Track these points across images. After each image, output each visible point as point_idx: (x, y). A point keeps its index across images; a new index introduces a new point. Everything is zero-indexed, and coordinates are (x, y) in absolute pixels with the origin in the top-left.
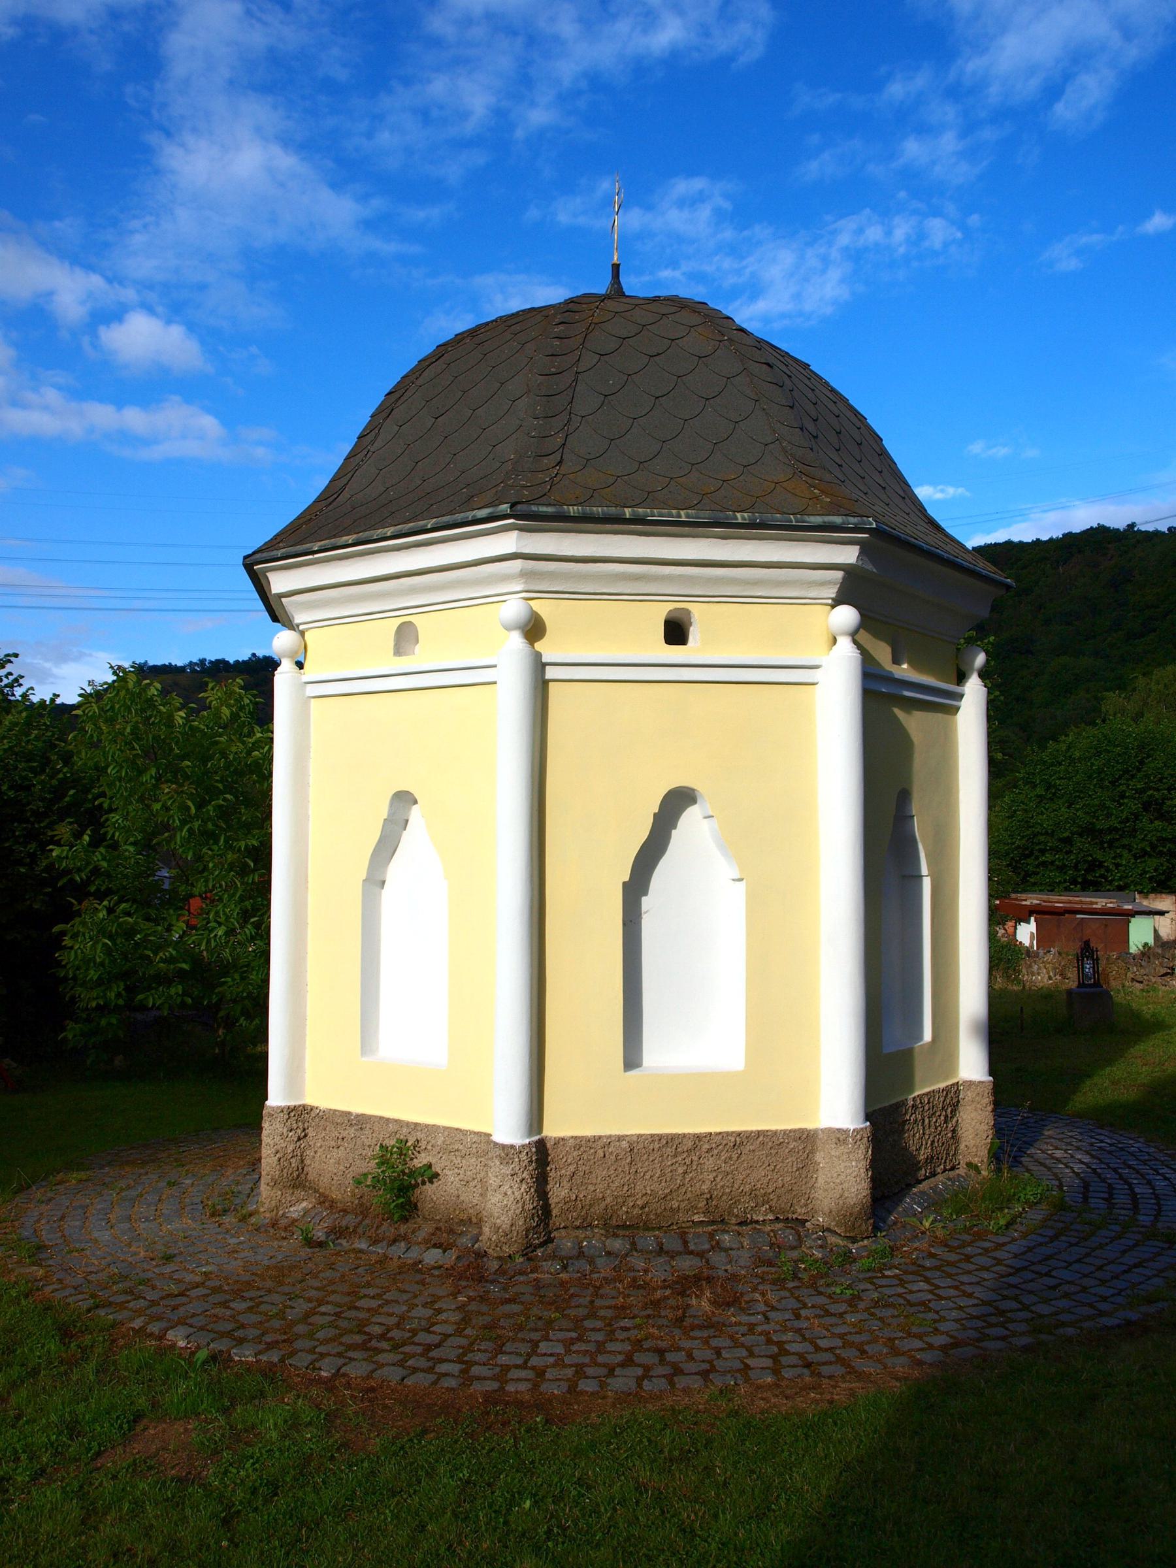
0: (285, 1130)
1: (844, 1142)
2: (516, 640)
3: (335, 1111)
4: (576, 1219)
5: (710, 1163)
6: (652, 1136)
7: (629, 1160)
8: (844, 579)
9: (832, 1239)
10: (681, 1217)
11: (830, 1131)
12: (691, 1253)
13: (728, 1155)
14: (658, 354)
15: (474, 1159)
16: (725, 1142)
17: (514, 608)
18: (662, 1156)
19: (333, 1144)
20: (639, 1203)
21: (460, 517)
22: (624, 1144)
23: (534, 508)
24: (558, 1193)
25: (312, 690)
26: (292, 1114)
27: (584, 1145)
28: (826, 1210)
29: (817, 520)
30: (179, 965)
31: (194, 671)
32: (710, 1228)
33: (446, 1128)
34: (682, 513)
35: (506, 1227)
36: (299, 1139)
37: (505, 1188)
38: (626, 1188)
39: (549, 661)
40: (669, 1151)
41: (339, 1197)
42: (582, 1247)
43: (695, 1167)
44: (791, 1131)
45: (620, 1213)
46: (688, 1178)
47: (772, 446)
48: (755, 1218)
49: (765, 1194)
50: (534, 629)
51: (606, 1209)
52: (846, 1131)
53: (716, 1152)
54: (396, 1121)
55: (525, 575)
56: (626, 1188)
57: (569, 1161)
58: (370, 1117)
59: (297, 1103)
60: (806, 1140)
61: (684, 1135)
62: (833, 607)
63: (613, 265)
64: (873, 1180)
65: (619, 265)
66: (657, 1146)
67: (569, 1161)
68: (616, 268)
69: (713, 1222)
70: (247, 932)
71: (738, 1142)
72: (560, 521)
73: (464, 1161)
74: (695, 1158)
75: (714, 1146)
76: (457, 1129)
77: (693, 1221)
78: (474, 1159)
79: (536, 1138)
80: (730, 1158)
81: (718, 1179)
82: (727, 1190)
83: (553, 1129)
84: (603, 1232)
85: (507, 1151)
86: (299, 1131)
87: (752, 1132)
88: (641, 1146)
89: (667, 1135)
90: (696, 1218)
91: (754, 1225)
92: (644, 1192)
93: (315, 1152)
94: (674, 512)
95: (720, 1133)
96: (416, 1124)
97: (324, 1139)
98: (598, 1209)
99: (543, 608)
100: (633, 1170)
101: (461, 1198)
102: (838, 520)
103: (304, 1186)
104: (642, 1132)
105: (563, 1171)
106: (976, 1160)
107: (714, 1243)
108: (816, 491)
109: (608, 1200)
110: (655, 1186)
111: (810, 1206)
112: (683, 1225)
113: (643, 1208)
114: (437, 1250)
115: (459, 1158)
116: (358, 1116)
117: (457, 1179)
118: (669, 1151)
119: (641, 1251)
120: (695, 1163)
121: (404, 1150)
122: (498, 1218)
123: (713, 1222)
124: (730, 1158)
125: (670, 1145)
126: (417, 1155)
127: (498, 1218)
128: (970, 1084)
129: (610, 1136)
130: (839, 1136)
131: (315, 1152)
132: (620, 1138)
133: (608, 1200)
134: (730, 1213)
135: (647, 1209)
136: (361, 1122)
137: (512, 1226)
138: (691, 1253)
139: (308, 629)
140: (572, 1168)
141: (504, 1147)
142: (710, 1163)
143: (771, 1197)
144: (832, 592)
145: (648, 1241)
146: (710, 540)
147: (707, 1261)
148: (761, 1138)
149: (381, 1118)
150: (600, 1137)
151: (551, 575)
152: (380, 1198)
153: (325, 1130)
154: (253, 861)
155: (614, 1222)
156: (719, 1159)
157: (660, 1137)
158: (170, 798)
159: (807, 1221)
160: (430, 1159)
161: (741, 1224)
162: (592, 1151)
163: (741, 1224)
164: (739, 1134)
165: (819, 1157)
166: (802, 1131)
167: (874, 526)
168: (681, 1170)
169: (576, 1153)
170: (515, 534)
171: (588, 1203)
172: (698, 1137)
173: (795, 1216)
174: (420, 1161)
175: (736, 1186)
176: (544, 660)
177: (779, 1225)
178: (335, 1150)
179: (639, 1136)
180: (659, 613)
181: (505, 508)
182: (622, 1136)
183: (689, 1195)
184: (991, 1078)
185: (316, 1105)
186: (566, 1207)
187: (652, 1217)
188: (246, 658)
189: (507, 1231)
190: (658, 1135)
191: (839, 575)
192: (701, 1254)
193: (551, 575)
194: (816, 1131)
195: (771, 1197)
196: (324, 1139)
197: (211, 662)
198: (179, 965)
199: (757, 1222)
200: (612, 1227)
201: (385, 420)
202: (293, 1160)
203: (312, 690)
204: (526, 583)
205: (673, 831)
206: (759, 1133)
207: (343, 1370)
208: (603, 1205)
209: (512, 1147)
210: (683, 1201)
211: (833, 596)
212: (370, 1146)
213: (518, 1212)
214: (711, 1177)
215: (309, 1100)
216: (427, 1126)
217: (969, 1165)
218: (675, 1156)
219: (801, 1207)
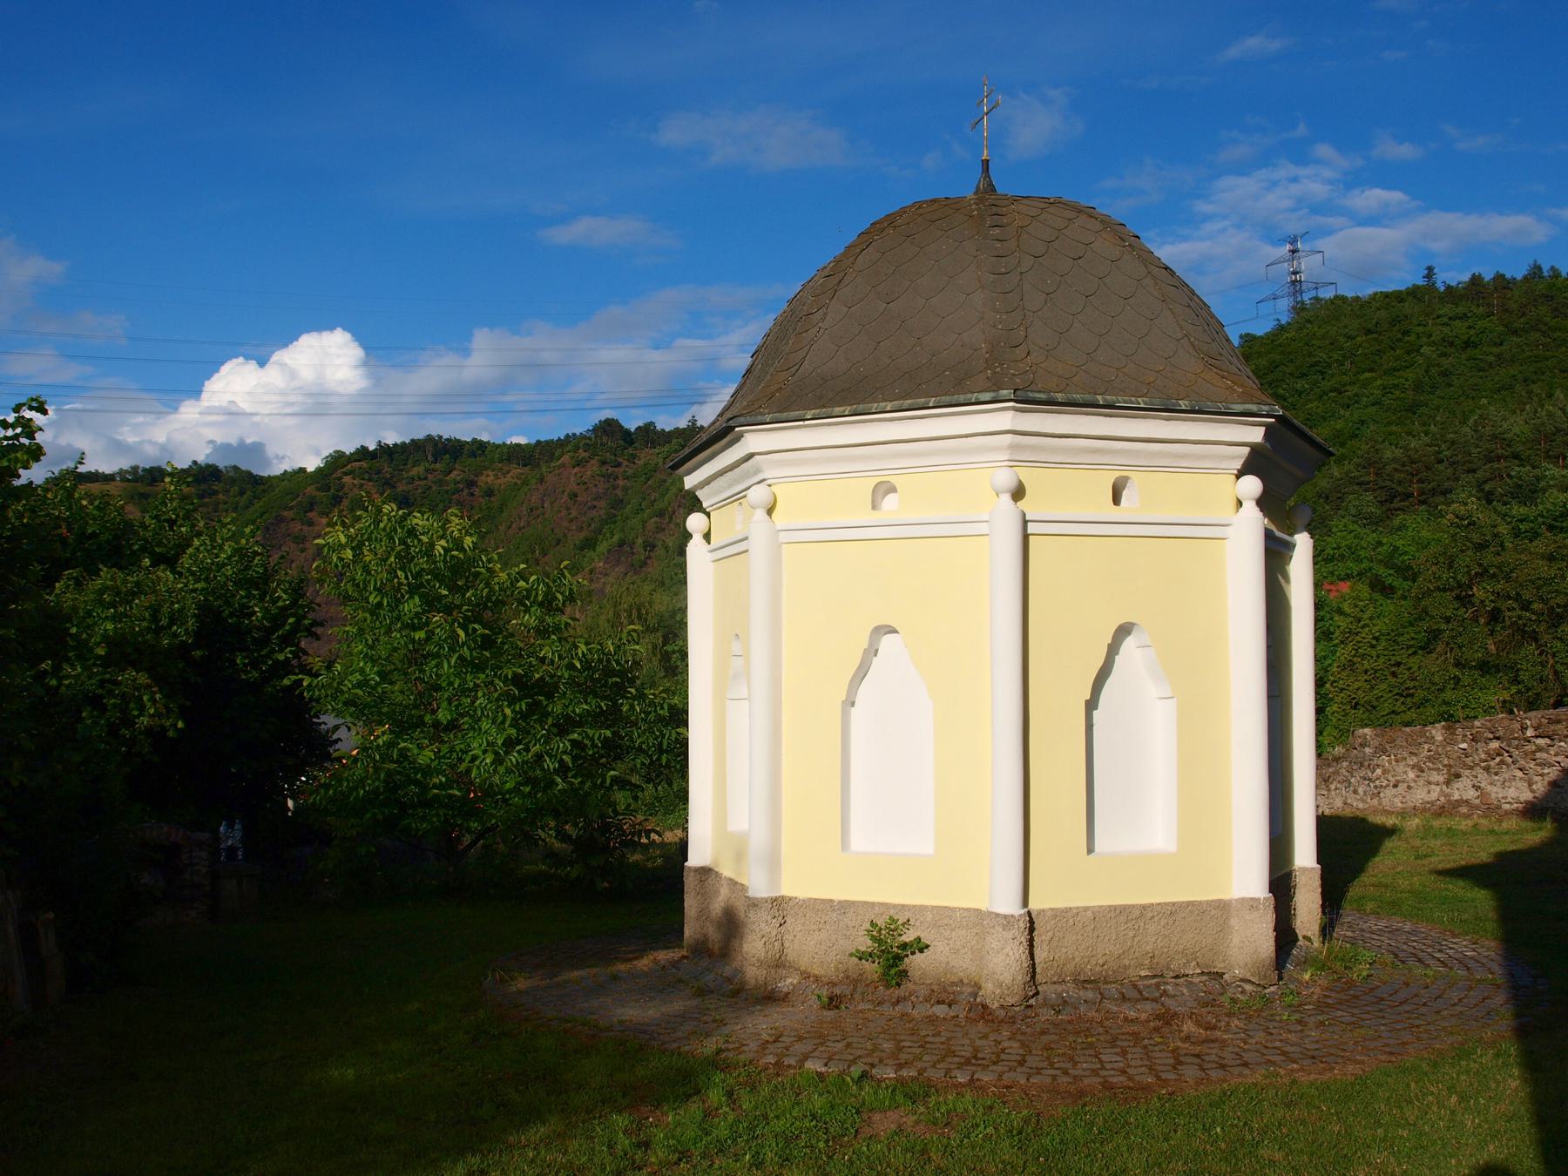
0: (769, 918)
1: (1257, 909)
2: (1006, 499)
3: (815, 900)
4: (1054, 976)
5: (1152, 928)
6: (1110, 906)
7: (1092, 927)
8: (1250, 454)
9: (1248, 987)
10: (1131, 972)
11: (1243, 901)
12: (1147, 999)
13: (1166, 921)
14: (1080, 258)
15: (964, 931)
16: (1163, 911)
17: (1006, 478)
18: (1117, 924)
19: (815, 927)
20: (1101, 962)
21: (955, 398)
22: (1089, 914)
23: (1031, 395)
24: (1041, 954)
25: (783, 537)
26: (775, 904)
27: (1060, 914)
28: (1242, 964)
29: (1238, 408)
30: (451, 792)
31: (124, 480)
32: (1153, 981)
33: (933, 907)
34: (1140, 400)
35: (1008, 980)
36: (781, 925)
37: (1008, 949)
38: (1090, 949)
39: (1031, 519)
40: (1123, 918)
41: (823, 972)
42: (1063, 997)
43: (1141, 931)
44: (1212, 901)
45: (1087, 970)
46: (1137, 939)
47: (1182, 341)
48: (1187, 972)
49: (1193, 953)
50: (1018, 493)
51: (1076, 967)
52: (1258, 900)
53: (1156, 919)
54: (882, 904)
55: (1013, 447)
56: (1090, 949)
57: (1048, 928)
58: (853, 903)
59: (778, 895)
60: (1222, 909)
61: (1133, 906)
62: (1238, 477)
63: (983, 161)
64: (1277, 938)
65: (988, 160)
66: (1113, 915)
67: (1048, 928)
68: (986, 163)
69: (1155, 976)
70: (514, 760)
71: (1173, 911)
72: (1051, 403)
73: (954, 933)
74: (1142, 924)
75: (1156, 914)
76: (946, 907)
77: (1140, 976)
78: (964, 931)
79: (1026, 910)
80: (1168, 923)
81: (1159, 941)
82: (1165, 950)
83: (1034, 905)
84: (1074, 986)
85: (1007, 920)
86: (780, 918)
87: (1183, 902)
88: (1102, 915)
89: (1120, 906)
90: (1143, 973)
91: (1186, 978)
92: (1104, 952)
93: (795, 936)
94: (1133, 399)
95: (1160, 904)
96: (903, 906)
97: (804, 924)
98: (1070, 968)
99: (1027, 475)
100: (1096, 935)
101: (951, 965)
102: (1254, 408)
103: (785, 966)
104: (1104, 903)
105: (1043, 937)
106: (1309, 934)
107: (1161, 991)
108: (1228, 382)
109: (1077, 960)
110: (1111, 948)
111: (1227, 962)
112: (1133, 979)
113: (1103, 965)
114: (942, 1006)
115: (949, 932)
116: (840, 902)
117: (947, 949)
118: (1123, 918)
119: (1109, 999)
120: (1142, 928)
121: (894, 927)
122: (1001, 974)
123: (1155, 976)
124: (1168, 923)
125: (1123, 914)
126: (906, 931)
127: (1001, 974)
128: (1304, 870)
129: (1078, 908)
130: (1252, 904)
131: (795, 936)
132: (1086, 909)
133: (1077, 960)
134: (1168, 968)
135: (1106, 967)
136: (845, 906)
137: (1013, 980)
138: (1147, 999)
139: (775, 484)
140: (1050, 934)
141: (1005, 917)
142: (1152, 928)
143: (1198, 955)
144: (1238, 464)
145: (1112, 990)
146: (1147, 420)
147: (1162, 1004)
148: (1190, 908)
149: (866, 903)
150: (1071, 908)
151: (1033, 448)
152: (872, 969)
153: (805, 916)
154: (518, 689)
155: (1082, 978)
156: (1159, 925)
157: (1115, 907)
158: (438, 627)
159: (1224, 974)
160: (918, 934)
161: (1177, 977)
162: (1065, 920)
163: (1177, 977)
164: (1174, 904)
165: (1234, 922)
166: (1220, 901)
167: (1281, 413)
168: (1131, 934)
169: (1053, 922)
170: (1011, 413)
171: (1062, 962)
172: (1144, 907)
173: (1215, 971)
174: (908, 937)
175: (1172, 946)
176: (1027, 518)
177: (1205, 978)
178: (817, 932)
179: (1101, 907)
180: (1109, 478)
181: (1004, 392)
182: (1088, 907)
183: (1137, 955)
184: (1319, 866)
185: (794, 896)
186: (1045, 966)
187: (1111, 973)
188: (186, 467)
189: (1009, 985)
190: (1114, 906)
191: (1247, 450)
192: (1154, 1000)
193: (1033, 448)
194: (1231, 901)
195: (1198, 955)
196: (804, 924)
197: (144, 470)
198: (451, 792)
199: (1187, 975)
200: (1084, 983)
201: (831, 299)
202: (776, 944)
203: (783, 537)
204: (1011, 454)
205: (1117, 657)
206: (1189, 903)
207: (976, 1077)
208: (1073, 964)
209: (1012, 916)
210: (1133, 959)
211: (1239, 467)
212: (854, 927)
213: (1017, 969)
214: (1154, 939)
215: (787, 890)
216: (914, 906)
217: (1305, 937)
218: (1126, 923)
219: (1220, 963)
